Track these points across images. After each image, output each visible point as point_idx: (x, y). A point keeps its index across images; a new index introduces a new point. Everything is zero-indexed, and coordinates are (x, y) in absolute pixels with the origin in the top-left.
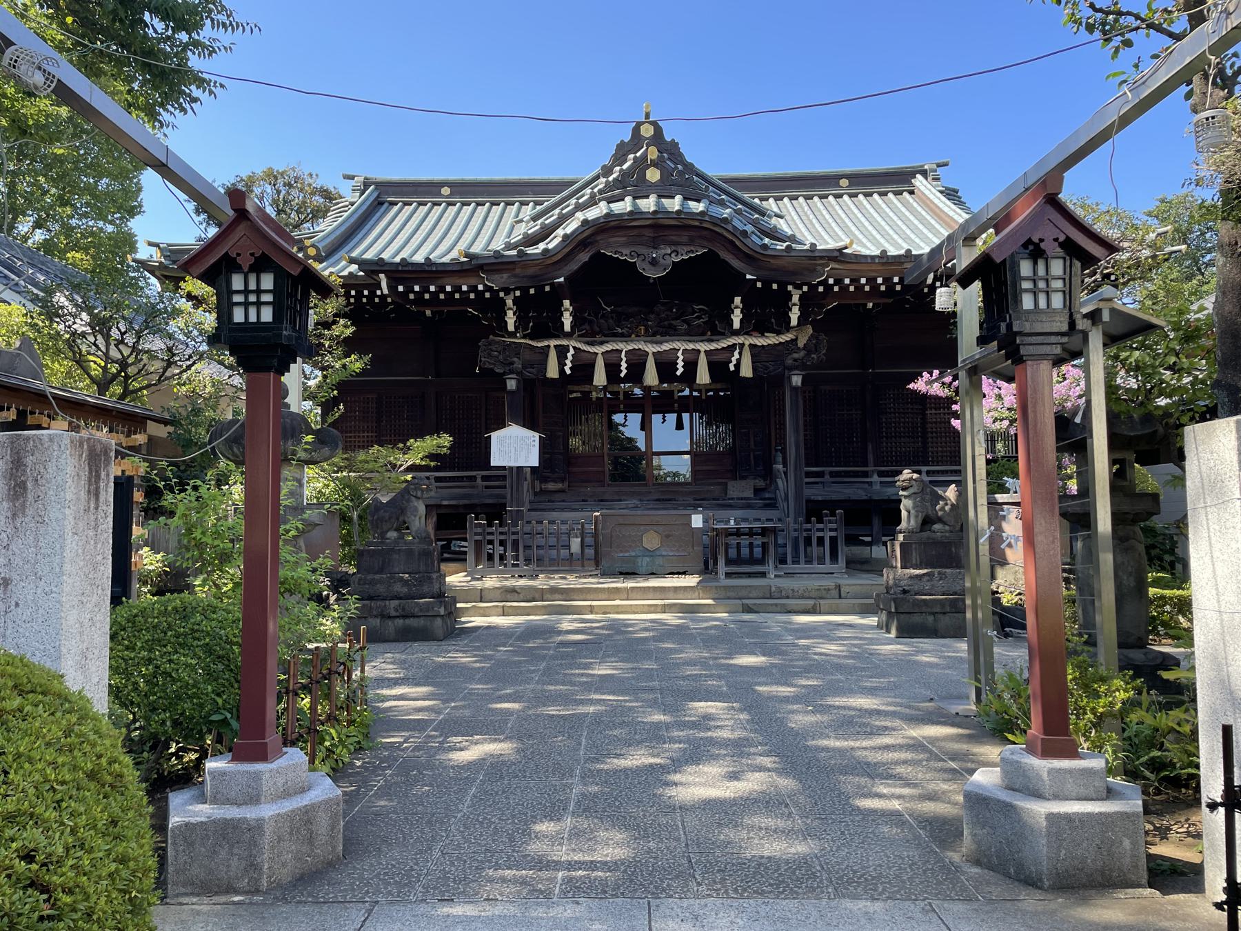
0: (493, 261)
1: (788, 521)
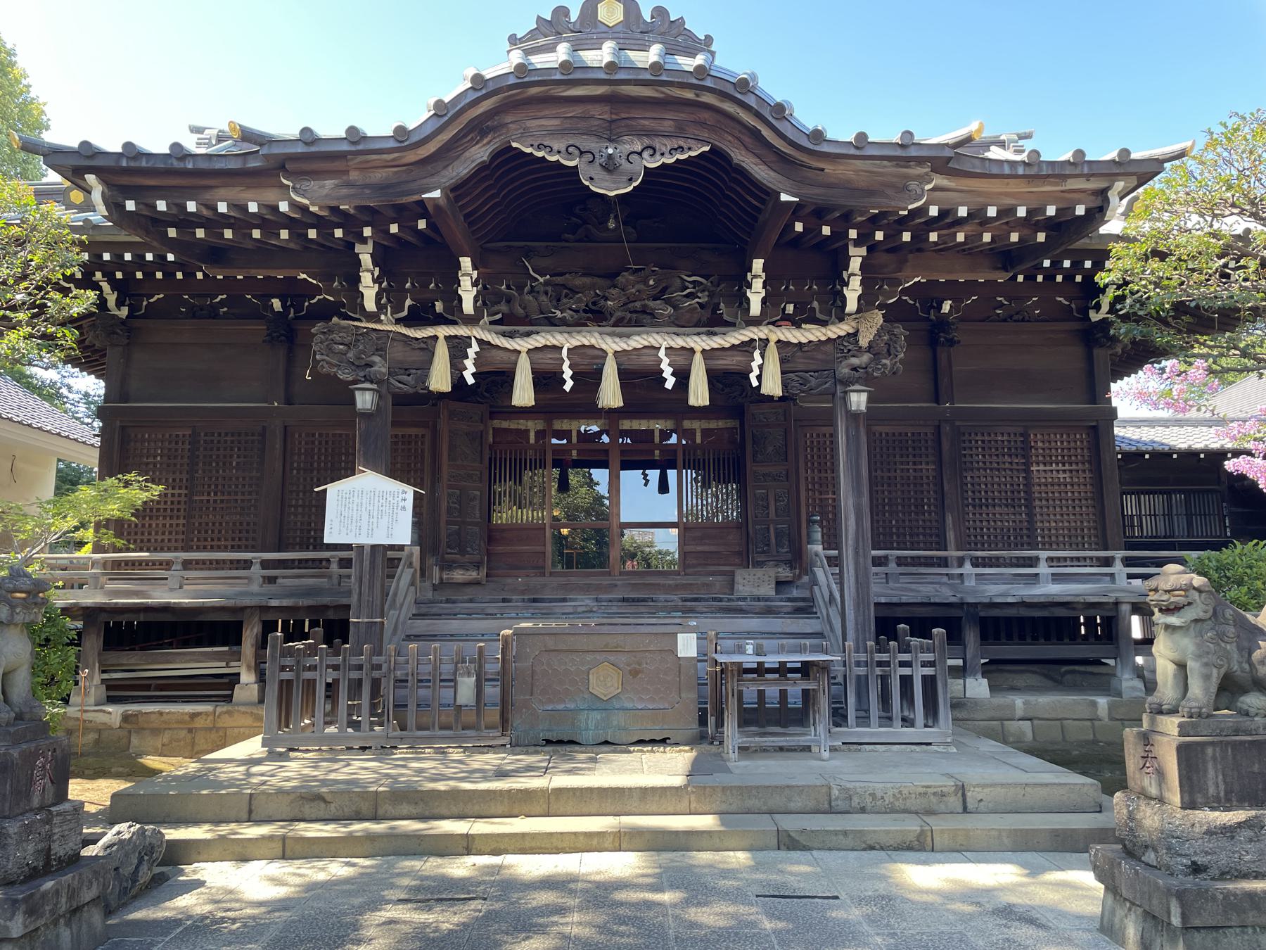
0: (300, 149)
1: (842, 648)
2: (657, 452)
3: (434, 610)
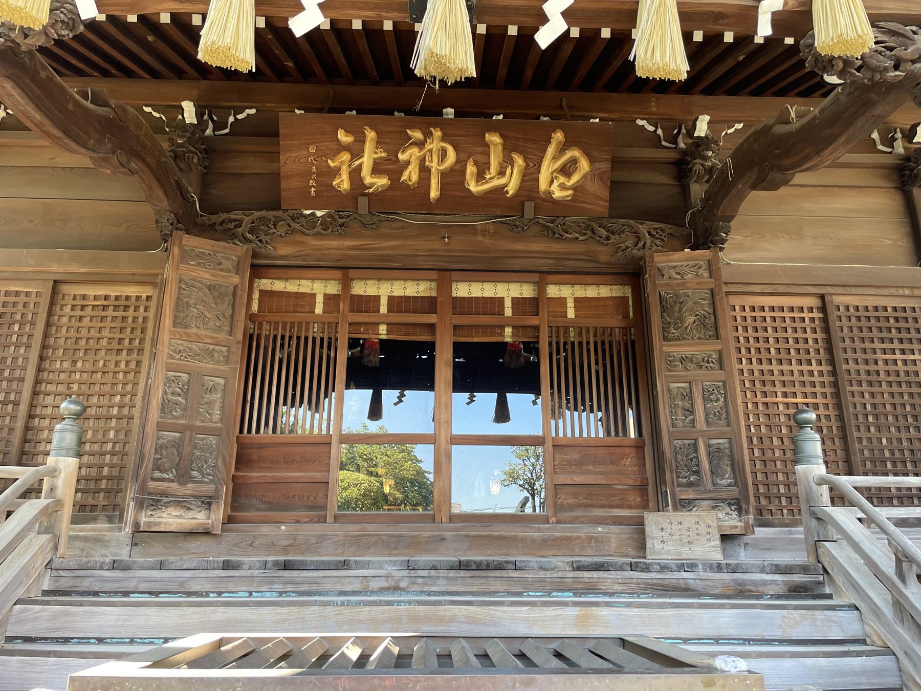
2: (508, 331)
3: (86, 584)
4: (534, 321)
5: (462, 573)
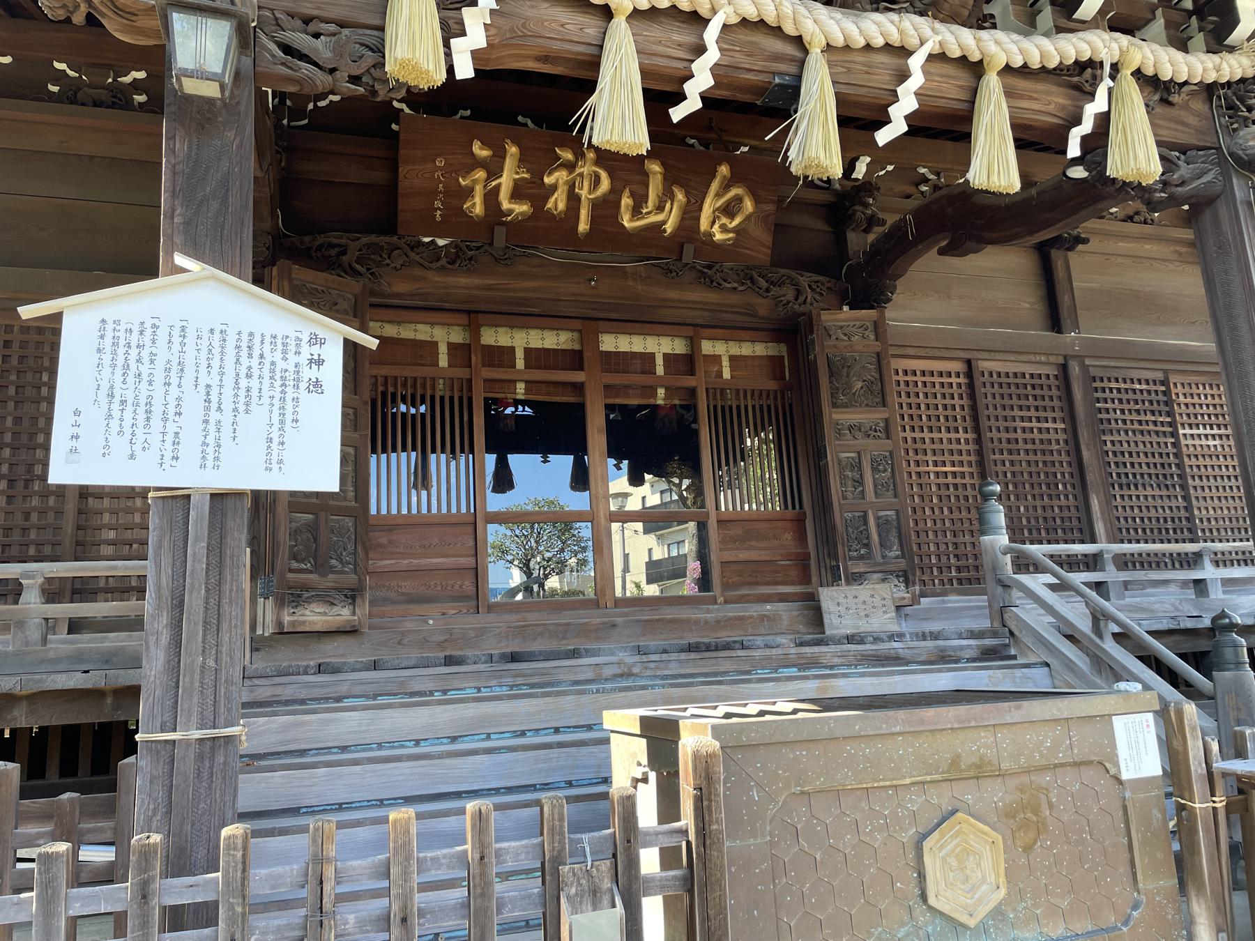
2: (661, 392)
3: (288, 692)
4: (690, 382)
5: (693, 655)
